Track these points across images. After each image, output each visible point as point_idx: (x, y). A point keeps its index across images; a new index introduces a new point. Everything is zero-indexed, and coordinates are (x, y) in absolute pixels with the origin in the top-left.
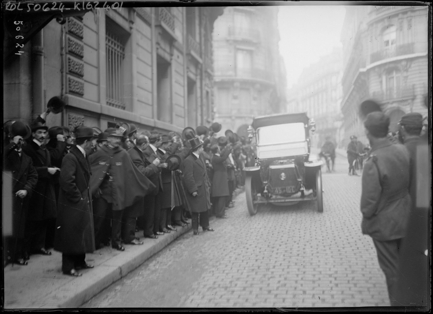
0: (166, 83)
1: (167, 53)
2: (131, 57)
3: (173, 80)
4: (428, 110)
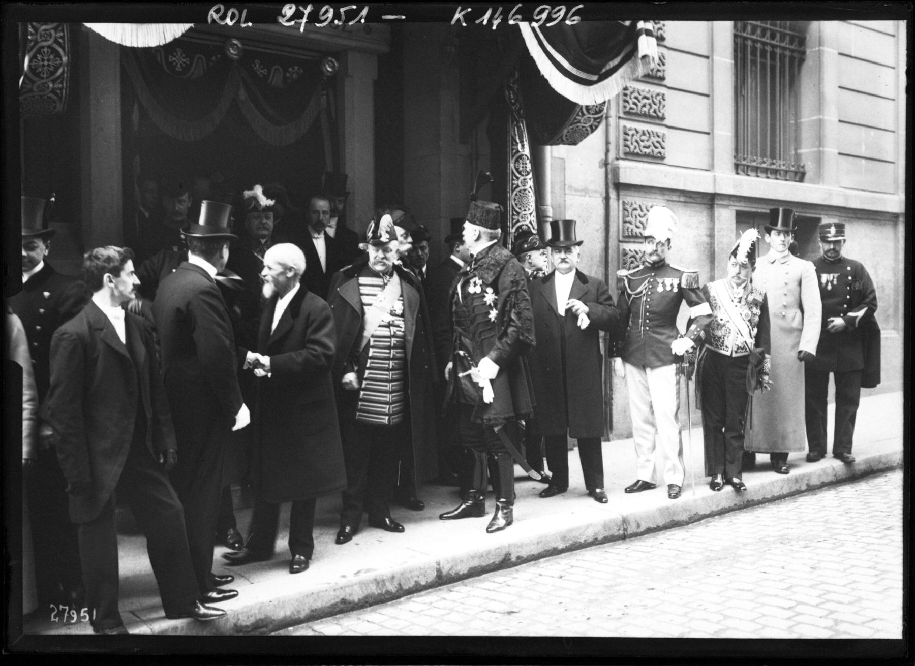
2: (820, 55)
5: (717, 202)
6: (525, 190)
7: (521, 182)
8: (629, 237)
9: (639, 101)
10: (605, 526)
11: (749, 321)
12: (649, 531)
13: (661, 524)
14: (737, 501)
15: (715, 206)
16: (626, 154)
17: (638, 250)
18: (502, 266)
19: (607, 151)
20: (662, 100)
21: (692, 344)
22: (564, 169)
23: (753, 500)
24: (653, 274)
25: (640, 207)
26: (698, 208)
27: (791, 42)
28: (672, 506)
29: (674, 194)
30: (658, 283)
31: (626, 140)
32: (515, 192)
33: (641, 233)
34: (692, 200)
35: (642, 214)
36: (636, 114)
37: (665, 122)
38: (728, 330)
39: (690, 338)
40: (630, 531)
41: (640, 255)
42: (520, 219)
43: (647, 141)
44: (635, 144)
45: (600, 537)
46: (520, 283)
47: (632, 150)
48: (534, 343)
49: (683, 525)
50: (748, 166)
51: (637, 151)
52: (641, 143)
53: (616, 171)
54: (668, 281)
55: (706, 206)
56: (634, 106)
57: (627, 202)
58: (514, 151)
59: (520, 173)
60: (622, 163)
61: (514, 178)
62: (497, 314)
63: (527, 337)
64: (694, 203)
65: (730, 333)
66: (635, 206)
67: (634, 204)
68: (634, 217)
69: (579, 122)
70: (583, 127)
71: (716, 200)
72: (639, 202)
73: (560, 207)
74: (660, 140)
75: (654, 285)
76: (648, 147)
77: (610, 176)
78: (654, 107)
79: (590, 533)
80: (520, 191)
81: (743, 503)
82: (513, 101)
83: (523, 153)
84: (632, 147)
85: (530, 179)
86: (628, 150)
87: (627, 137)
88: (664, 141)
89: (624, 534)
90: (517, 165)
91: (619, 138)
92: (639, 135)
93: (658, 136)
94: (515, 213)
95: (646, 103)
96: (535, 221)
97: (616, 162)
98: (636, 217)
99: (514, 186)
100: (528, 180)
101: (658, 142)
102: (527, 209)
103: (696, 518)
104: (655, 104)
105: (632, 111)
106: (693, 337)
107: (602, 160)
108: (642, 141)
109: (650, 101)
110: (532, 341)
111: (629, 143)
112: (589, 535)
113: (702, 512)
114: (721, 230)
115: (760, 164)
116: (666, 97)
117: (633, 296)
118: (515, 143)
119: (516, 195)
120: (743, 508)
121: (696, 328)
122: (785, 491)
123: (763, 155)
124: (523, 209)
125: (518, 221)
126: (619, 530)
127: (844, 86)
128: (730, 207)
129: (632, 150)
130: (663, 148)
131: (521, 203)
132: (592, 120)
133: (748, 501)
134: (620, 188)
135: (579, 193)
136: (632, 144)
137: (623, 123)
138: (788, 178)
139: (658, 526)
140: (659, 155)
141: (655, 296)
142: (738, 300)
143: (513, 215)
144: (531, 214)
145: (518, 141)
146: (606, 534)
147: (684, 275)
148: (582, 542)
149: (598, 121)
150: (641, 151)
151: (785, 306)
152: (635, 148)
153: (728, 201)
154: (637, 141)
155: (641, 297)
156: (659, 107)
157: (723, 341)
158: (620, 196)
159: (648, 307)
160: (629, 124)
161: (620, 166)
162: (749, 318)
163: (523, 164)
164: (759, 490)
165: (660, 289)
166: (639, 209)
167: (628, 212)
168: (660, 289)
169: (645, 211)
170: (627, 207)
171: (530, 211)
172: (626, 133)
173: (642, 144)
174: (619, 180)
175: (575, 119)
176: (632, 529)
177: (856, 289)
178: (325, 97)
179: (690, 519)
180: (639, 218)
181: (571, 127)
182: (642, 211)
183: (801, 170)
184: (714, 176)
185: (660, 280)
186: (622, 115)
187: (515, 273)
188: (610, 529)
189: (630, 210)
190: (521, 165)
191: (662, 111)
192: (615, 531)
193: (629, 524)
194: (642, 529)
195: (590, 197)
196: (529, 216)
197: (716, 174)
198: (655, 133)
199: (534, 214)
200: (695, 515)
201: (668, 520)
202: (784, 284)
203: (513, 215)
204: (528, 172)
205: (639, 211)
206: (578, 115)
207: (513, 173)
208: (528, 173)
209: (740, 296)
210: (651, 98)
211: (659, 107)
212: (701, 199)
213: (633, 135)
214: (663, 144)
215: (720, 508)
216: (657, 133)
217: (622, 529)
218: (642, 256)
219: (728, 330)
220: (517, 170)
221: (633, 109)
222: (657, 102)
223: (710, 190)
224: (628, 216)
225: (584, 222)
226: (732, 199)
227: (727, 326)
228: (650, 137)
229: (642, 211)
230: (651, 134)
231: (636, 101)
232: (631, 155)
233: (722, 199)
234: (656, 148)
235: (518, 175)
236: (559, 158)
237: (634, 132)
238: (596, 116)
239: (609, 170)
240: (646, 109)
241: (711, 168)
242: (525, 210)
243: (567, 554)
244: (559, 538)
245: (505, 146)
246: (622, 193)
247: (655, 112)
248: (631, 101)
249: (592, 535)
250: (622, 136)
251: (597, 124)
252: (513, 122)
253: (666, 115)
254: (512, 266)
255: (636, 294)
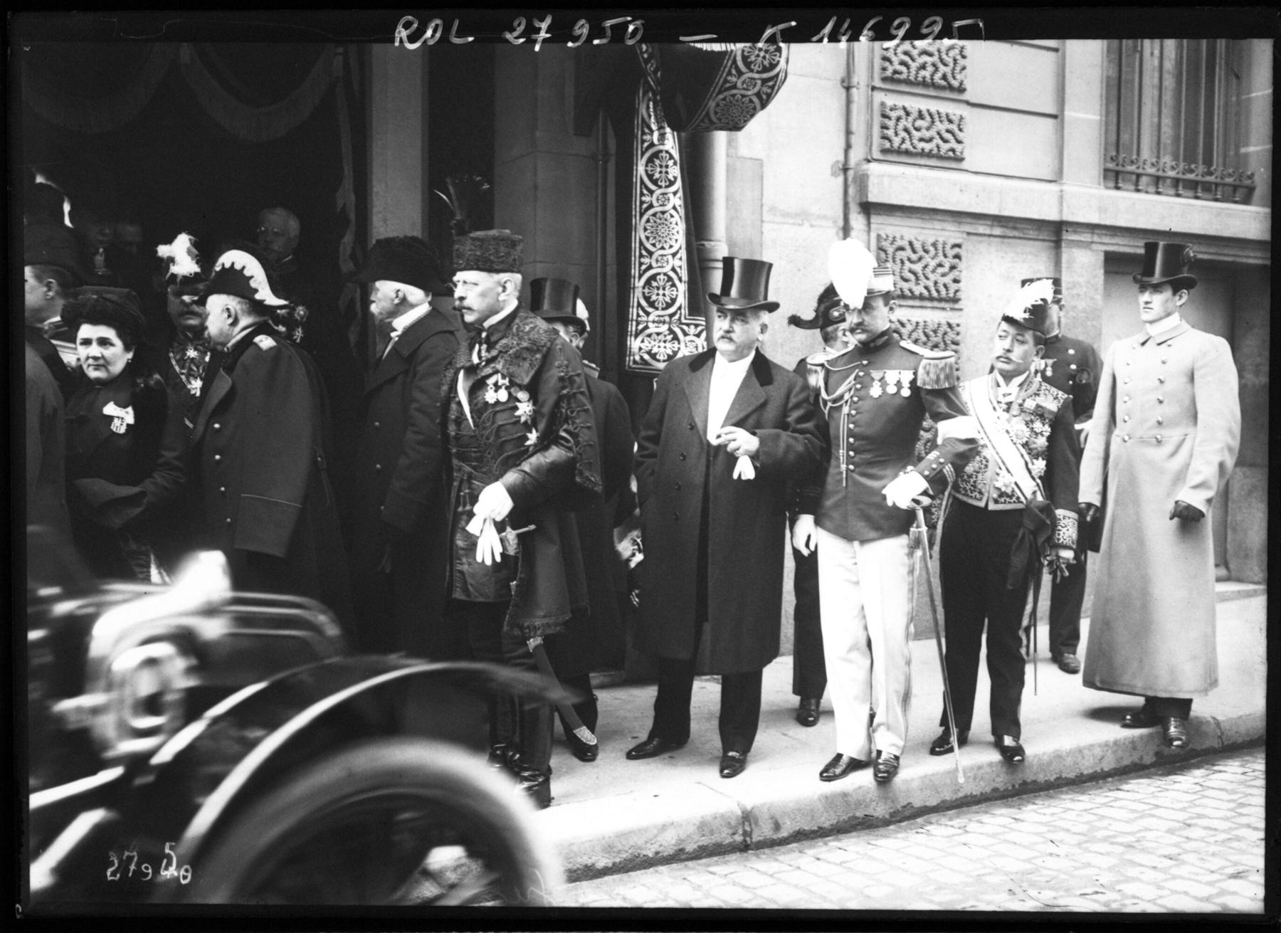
5: (1066, 236)
6: (663, 213)
7: (658, 200)
9: (913, 60)
10: (703, 826)
11: (1026, 445)
12: (801, 836)
13: (827, 825)
14: (1002, 780)
15: (1063, 244)
16: (884, 151)
17: (904, 320)
18: (545, 349)
19: (848, 147)
20: (958, 57)
21: (924, 485)
22: (762, 177)
23: (1034, 782)
24: (865, 362)
25: (911, 244)
26: (1030, 247)
28: (855, 790)
29: (981, 222)
30: (873, 379)
31: (884, 127)
32: (645, 217)
33: (910, 290)
34: (1016, 233)
35: (914, 257)
36: (907, 82)
37: (966, 96)
38: (984, 462)
39: (921, 474)
40: (756, 837)
41: (910, 327)
42: (654, 264)
43: (928, 129)
44: (903, 134)
45: (690, 847)
46: (575, 381)
47: (896, 145)
48: (599, 489)
49: (877, 827)
51: (907, 145)
52: (914, 132)
53: (862, 181)
54: (892, 376)
55: (1047, 244)
56: (903, 69)
57: (884, 236)
58: (646, 145)
59: (655, 182)
60: (874, 168)
61: (645, 192)
62: (538, 437)
63: (587, 478)
64: (1020, 238)
65: (986, 466)
66: (899, 243)
67: (897, 239)
68: (898, 262)
69: (734, 87)
70: (743, 96)
71: (1064, 232)
72: (907, 237)
73: (751, 243)
74: (954, 127)
75: (865, 383)
76: (930, 140)
77: (851, 191)
78: (942, 69)
79: (669, 839)
80: (654, 215)
81: (1013, 786)
82: (646, 56)
83: (661, 147)
84: (897, 141)
85: (675, 193)
86: (888, 145)
87: (886, 121)
88: (961, 130)
89: (745, 841)
90: (649, 169)
91: (872, 125)
92: (910, 119)
93: (950, 121)
94: (644, 253)
95: (926, 63)
96: (685, 266)
97: (865, 166)
98: (902, 262)
99: (645, 206)
100: (671, 196)
101: (948, 131)
102: (666, 246)
103: (907, 813)
104: (945, 65)
105: (897, 76)
106: (927, 473)
107: (838, 162)
108: (918, 129)
109: (935, 59)
110: (595, 484)
111: (890, 133)
112: (668, 841)
113: (918, 803)
114: (1075, 286)
115: (1184, 174)
116: (966, 52)
117: (830, 404)
118: (647, 131)
119: (648, 221)
120: (1013, 796)
121: (938, 457)
122: (1107, 766)
124: (659, 246)
125: (650, 267)
126: (734, 834)
128: (1094, 247)
129: (896, 145)
130: (959, 142)
131: (655, 234)
132: (759, 82)
133: (1024, 783)
134: (872, 211)
135: (792, 221)
136: (896, 134)
137: (879, 97)
138: (1219, 197)
139: (820, 828)
140: (951, 154)
141: (865, 405)
142: (1005, 407)
143: (641, 256)
144: (674, 255)
145: (654, 127)
146: (705, 841)
147: (924, 362)
148: (651, 855)
149: (771, 84)
150: (914, 148)
151: (1159, 423)
152: (903, 141)
153: (1090, 235)
154: (906, 130)
155: (841, 406)
156: (954, 69)
157: (975, 482)
158: (873, 226)
159: (851, 426)
160: (891, 100)
161: (869, 173)
162: (1024, 440)
163: (661, 166)
164: (1050, 764)
165: (875, 391)
166: (908, 247)
167: (886, 254)
168: (875, 391)
169: (921, 253)
170: (885, 244)
171: (673, 250)
172: (884, 116)
173: (916, 134)
174: (867, 197)
175: (726, 81)
176: (763, 831)
177: (1084, 381)
178: (340, 58)
179: (892, 815)
180: (908, 264)
181: (721, 96)
182: (914, 251)
183: (1248, 182)
184: (1062, 191)
185: (876, 374)
186: (878, 83)
187: (566, 362)
188: (712, 833)
189: (890, 250)
190: (658, 169)
191: (958, 77)
192: (724, 835)
193: (756, 823)
194: (784, 833)
195: (812, 226)
196: (670, 257)
197: (1065, 188)
198: (943, 115)
199: (683, 254)
200: (904, 807)
201: (845, 817)
203: (641, 256)
204: (670, 180)
205: (909, 252)
206: (730, 73)
207: (642, 182)
208: (671, 183)
209: (1008, 399)
210: (936, 53)
211: (954, 69)
212: (1036, 233)
213: (899, 119)
214: (960, 135)
215: (961, 795)
216: (947, 115)
217: (740, 831)
218: (913, 331)
219: (984, 462)
220: (650, 177)
221: (900, 73)
222: (949, 60)
223: (1052, 215)
224: (886, 261)
225: (799, 270)
226: (1096, 231)
227: (983, 454)
228: (933, 122)
229: (914, 251)
230: (936, 116)
231: (907, 59)
232: (893, 153)
233: (1075, 232)
234: (946, 141)
235: (652, 187)
236: (751, 159)
237: (902, 113)
238: (765, 76)
239: (850, 179)
240: (926, 74)
241: (1057, 177)
242: (663, 248)
243: (615, 877)
244: (598, 848)
245: (633, 136)
246: (874, 219)
247: (944, 77)
248: (894, 59)
249: (673, 842)
250: (877, 120)
251: (769, 91)
252: (645, 93)
253: (967, 84)
254: (560, 349)
255: (835, 401)
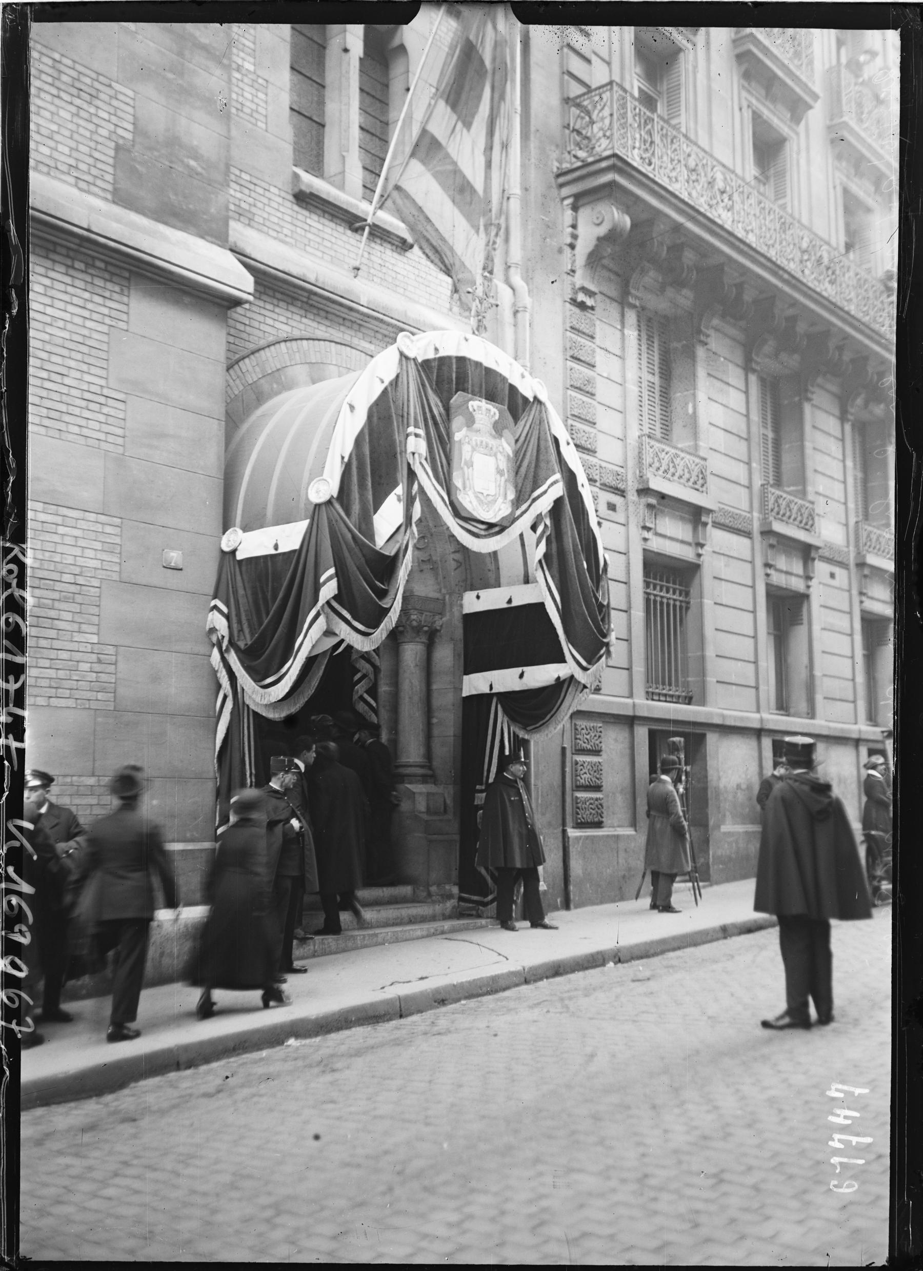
0: (799, 635)
1: (797, 576)
2: (701, 606)
3: (816, 628)
4: (32, 201)
8: (579, 750)
27: (680, 595)
50: (653, 693)
123: (664, 684)
127: (598, 52)
202: (348, 47)
241: (631, 696)
